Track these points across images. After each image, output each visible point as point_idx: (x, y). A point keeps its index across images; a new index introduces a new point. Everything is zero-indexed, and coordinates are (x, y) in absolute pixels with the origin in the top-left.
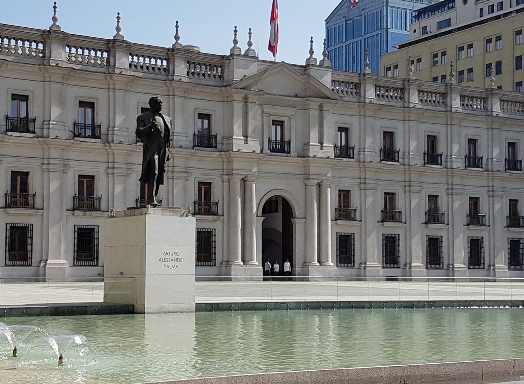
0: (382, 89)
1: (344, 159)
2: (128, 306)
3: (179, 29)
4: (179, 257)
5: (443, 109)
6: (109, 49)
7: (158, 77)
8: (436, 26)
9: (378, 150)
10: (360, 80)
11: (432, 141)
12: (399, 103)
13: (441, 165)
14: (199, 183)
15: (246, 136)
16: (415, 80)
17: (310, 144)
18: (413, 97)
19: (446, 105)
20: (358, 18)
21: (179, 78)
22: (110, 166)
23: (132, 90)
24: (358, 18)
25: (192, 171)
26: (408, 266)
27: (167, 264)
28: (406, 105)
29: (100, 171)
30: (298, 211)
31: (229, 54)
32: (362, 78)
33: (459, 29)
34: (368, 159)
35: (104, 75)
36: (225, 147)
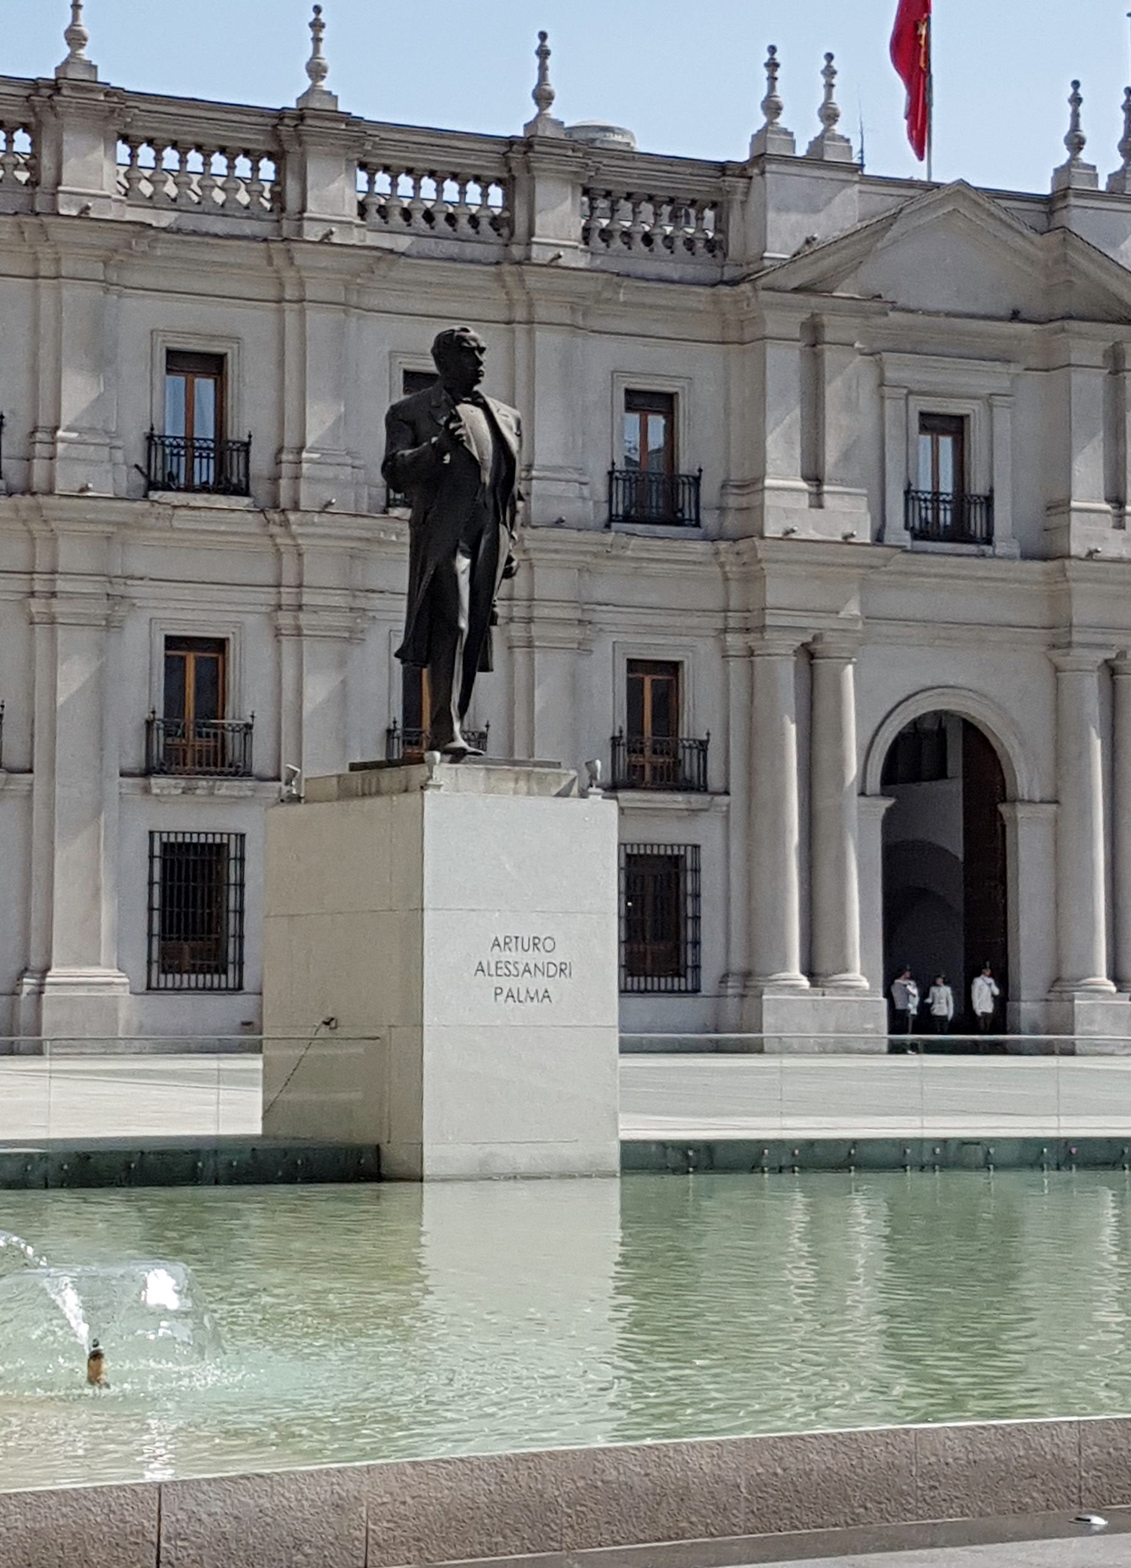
4: (558, 958)
14: (633, 665)
15: (815, 478)
17: (1074, 504)
25: (602, 615)
27: (507, 984)
30: (1026, 776)
36: (732, 522)
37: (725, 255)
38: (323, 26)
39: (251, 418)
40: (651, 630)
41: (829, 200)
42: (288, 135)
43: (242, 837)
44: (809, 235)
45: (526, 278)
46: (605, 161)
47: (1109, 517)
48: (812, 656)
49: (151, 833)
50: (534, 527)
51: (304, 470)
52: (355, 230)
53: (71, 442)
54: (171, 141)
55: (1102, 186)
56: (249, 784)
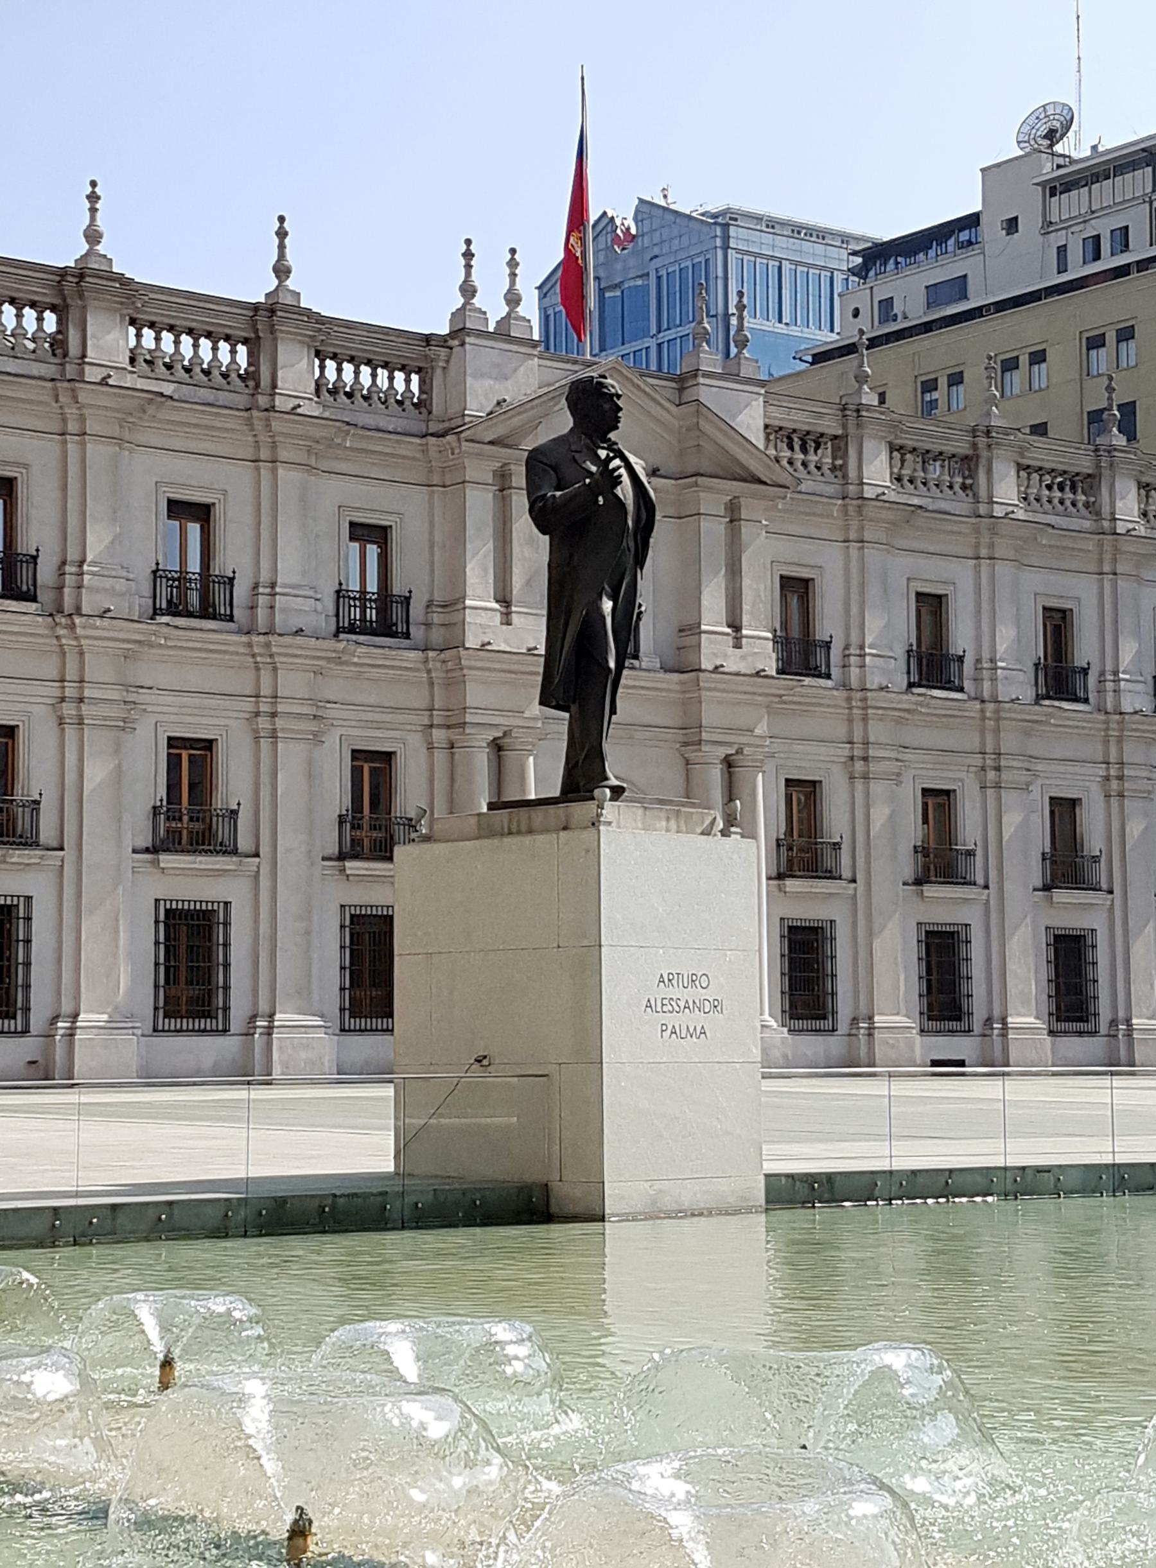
0: (908, 456)
1: (807, 681)
2: (526, 1190)
3: (287, 241)
5: (1087, 524)
6: (64, 300)
7: (223, 397)
8: (921, 296)
9: (900, 651)
10: (844, 427)
11: (1058, 625)
12: (960, 504)
13: (1086, 701)
14: (356, 754)
15: (505, 601)
16: (1006, 431)
17: (703, 627)
18: (1003, 484)
19: (1098, 513)
20: (639, 282)
21: (292, 403)
22: (68, 692)
23: (141, 438)
24: (639, 282)
25: (332, 712)
26: (996, 1024)
27: (672, 1020)
28: (983, 509)
29: (35, 709)
31: (447, 332)
32: (851, 422)
33: (1001, 306)
34: (874, 681)
35: (49, 384)
36: (437, 636)
37: (430, 413)
38: (98, 198)
39: (233, 556)
40: (378, 725)
41: (515, 370)
42: (264, 323)
43: (29, 898)
44: (500, 398)
45: (273, 423)
46: (336, 328)
47: (730, 638)
48: (500, 749)
49: (157, 901)
50: (280, 635)
51: (85, 582)
52: (129, 376)
53: (93, 574)
54: (31, 301)
55: (491, 329)
56: (37, 852)
